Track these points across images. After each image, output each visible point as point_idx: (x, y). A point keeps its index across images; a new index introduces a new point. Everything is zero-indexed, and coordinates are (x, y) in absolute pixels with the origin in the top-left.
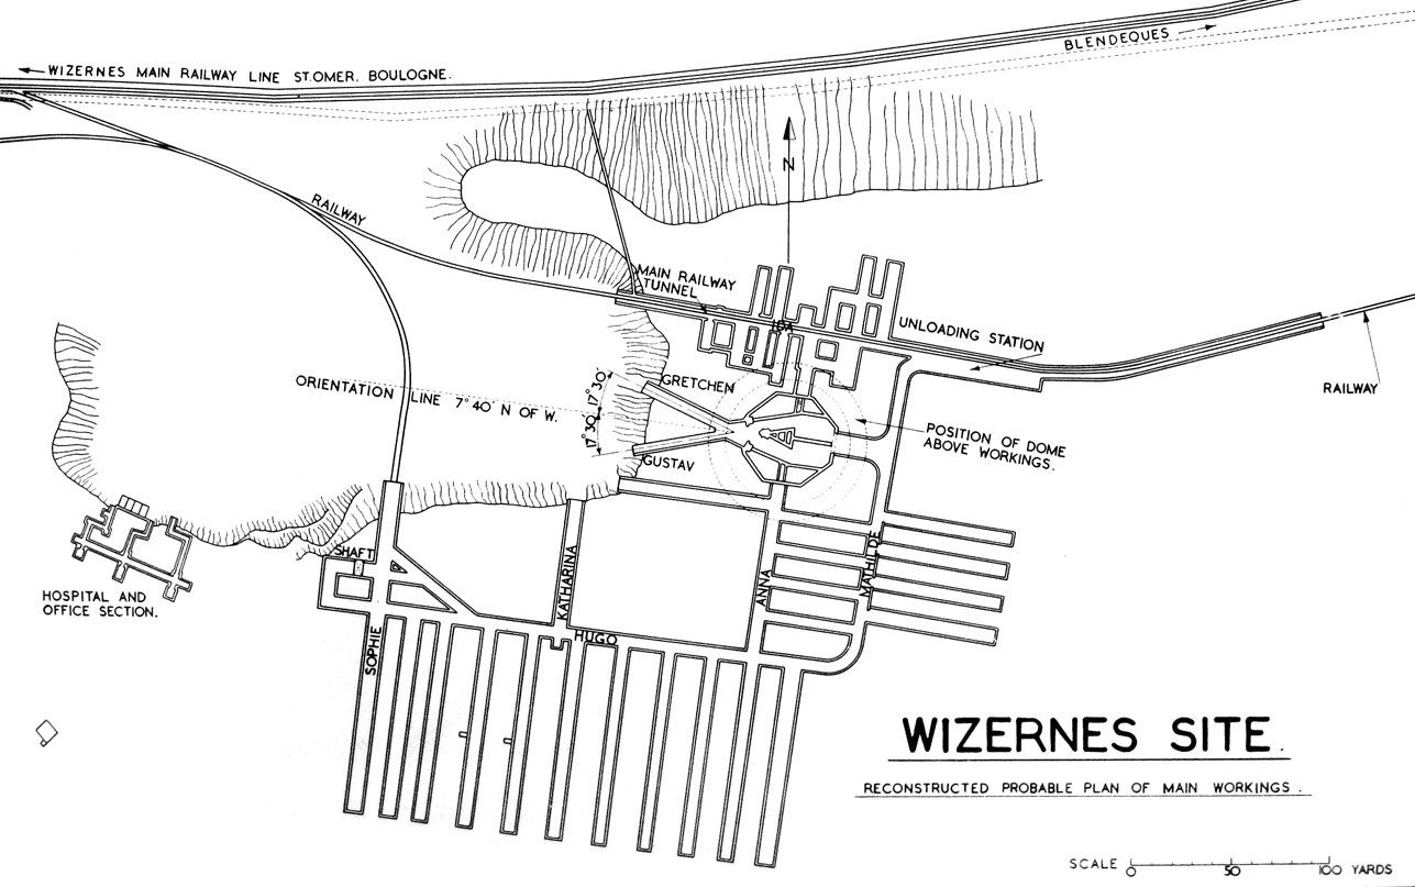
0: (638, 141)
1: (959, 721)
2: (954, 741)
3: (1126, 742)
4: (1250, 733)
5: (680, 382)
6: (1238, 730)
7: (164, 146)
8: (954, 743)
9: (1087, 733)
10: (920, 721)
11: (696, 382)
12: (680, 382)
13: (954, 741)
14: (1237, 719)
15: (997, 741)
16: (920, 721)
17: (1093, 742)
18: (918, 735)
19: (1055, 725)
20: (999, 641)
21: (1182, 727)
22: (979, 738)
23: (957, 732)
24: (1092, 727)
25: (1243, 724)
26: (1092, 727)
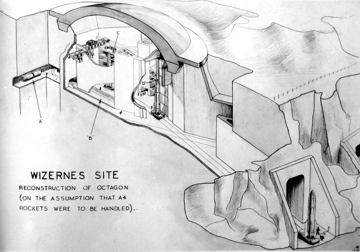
0: (222, 113)
1: (43, 172)
2: (42, 177)
3: (82, 177)
4: (114, 174)
5: (67, 209)
6: (111, 174)
7: (20, 112)
8: (41, 177)
9: (72, 175)
10: (56, 208)
11: (80, 208)
12: (67, 209)
13: (42, 177)
14: (111, 172)
15: (51, 177)
16: (56, 208)
17: (74, 177)
18: (34, 175)
19: (69, 178)
20: (115, 211)
21: (97, 173)
22: (47, 176)
23: (42, 175)
24: (73, 173)
25: (112, 173)
26: (73, 173)
